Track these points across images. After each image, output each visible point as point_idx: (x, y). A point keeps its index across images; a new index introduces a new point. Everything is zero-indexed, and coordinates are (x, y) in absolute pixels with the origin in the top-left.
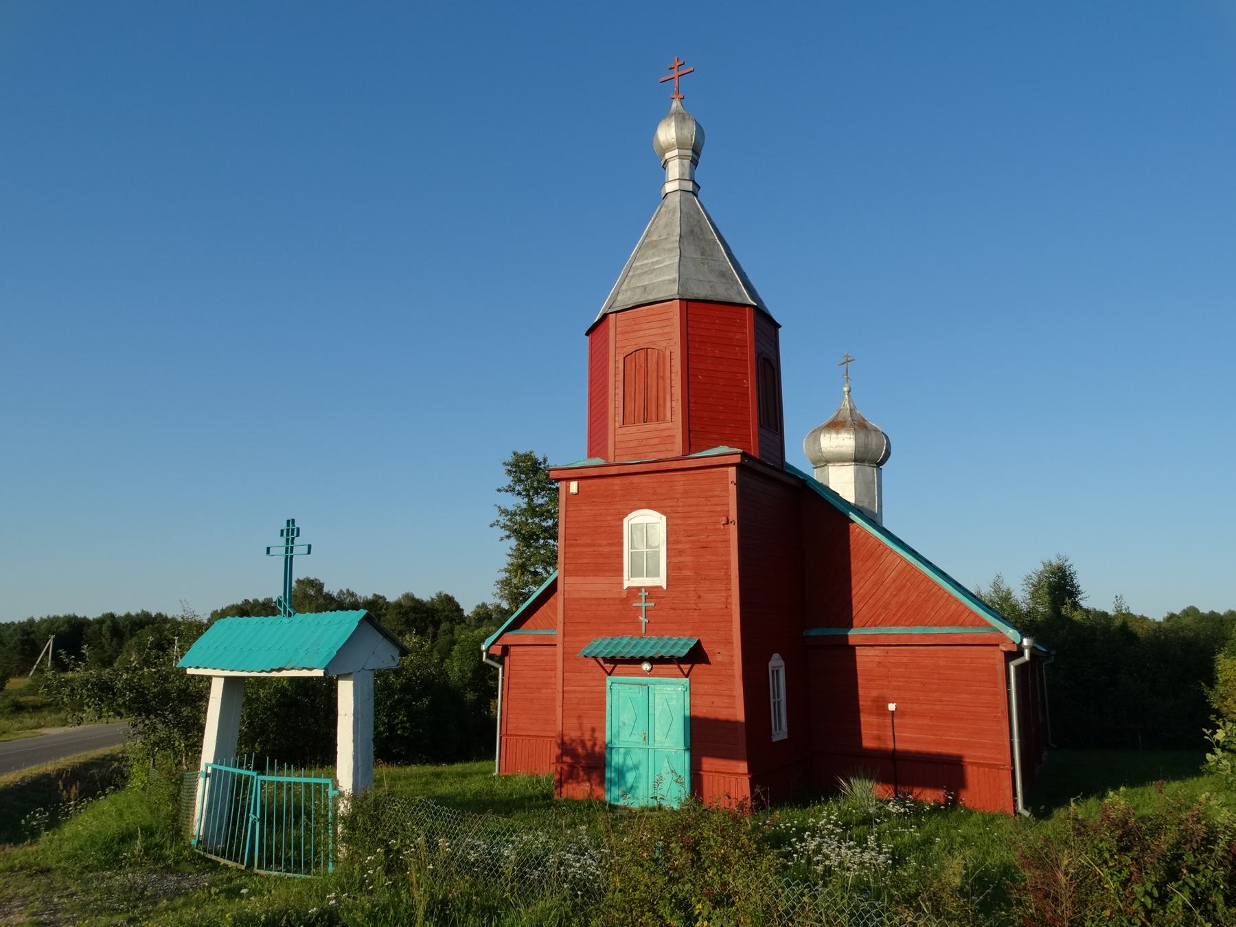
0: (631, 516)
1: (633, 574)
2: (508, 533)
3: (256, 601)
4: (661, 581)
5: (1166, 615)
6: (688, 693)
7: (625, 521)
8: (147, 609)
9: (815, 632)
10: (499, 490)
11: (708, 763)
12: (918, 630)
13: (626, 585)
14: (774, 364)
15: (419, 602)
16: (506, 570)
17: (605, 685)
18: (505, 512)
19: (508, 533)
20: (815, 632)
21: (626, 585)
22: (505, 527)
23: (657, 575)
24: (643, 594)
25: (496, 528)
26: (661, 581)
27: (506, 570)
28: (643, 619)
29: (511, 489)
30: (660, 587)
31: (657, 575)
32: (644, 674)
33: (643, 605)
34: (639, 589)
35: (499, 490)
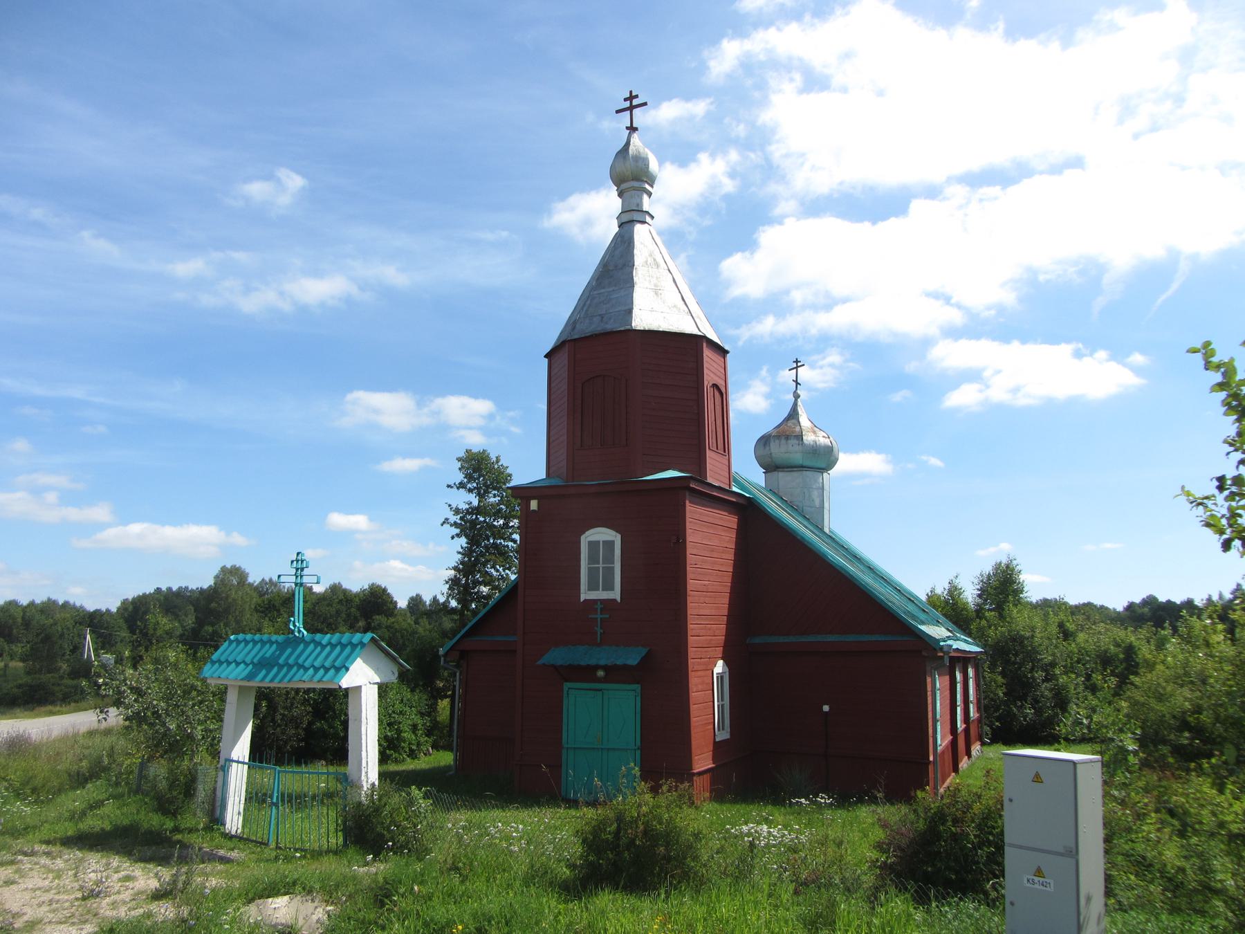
0: (588, 533)
1: (593, 586)
2: (458, 531)
3: (170, 589)
4: (616, 594)
5: (1126, 604)
6: (639, 699)
7: (583, 538)
8: (54, 597)
9: (757, 640)
10: (449, 486)
11: (1073, 845)
12: (851, 638)
13: (583, 598)
14: (723, 390)
15: (345, 592)
16: (455, 568)
17: (562, 690)
18: (457, 511)
19: (458, 531)
20: (757, 640)
21: (583, 598)
22: (455, 525)
23: (612, 588)
24: (599, 606)
25: (447, 526)
26: (616, 594)
27: (455, 568)
28: (599, 631)
29: (461, 486)
30: (615, 600)
31: (612, 588)
32: (599, 680)
33: (599, 616)
34: (595, 601)
35: (449, 486)
